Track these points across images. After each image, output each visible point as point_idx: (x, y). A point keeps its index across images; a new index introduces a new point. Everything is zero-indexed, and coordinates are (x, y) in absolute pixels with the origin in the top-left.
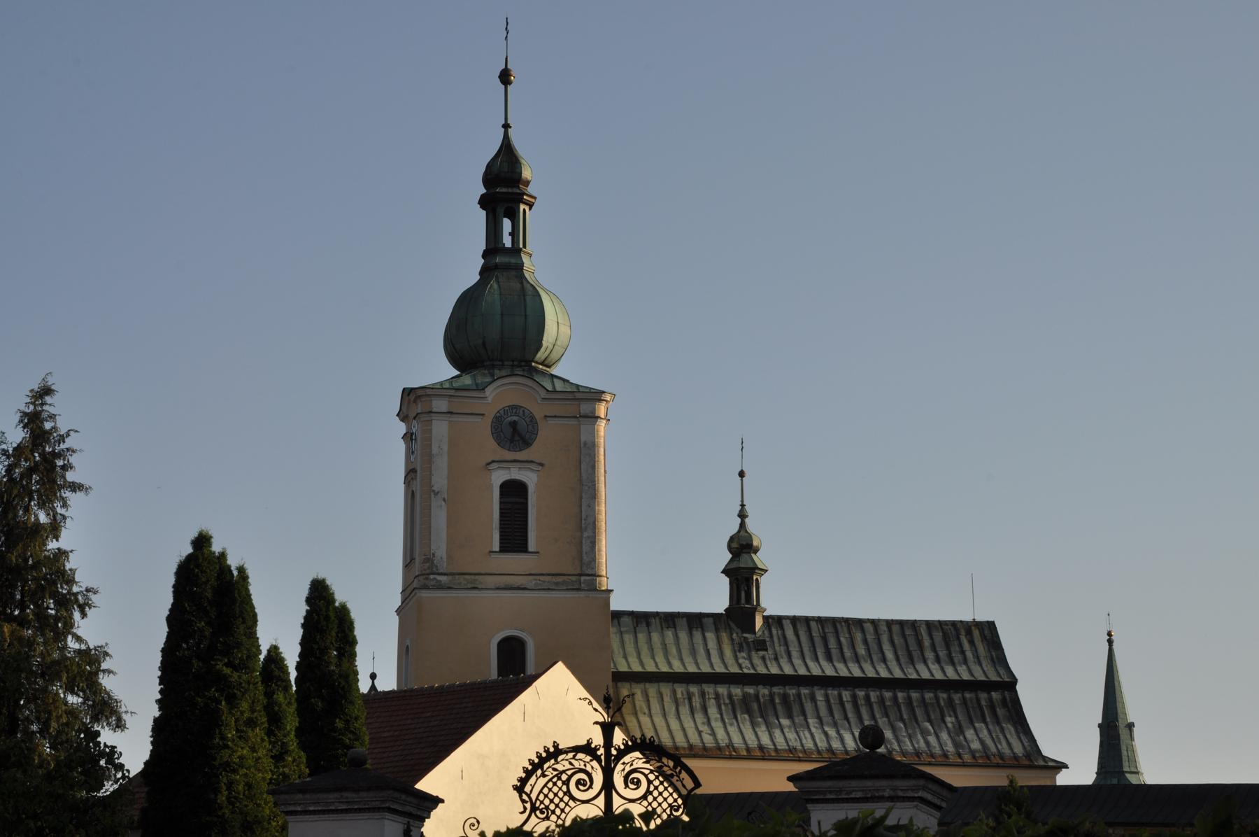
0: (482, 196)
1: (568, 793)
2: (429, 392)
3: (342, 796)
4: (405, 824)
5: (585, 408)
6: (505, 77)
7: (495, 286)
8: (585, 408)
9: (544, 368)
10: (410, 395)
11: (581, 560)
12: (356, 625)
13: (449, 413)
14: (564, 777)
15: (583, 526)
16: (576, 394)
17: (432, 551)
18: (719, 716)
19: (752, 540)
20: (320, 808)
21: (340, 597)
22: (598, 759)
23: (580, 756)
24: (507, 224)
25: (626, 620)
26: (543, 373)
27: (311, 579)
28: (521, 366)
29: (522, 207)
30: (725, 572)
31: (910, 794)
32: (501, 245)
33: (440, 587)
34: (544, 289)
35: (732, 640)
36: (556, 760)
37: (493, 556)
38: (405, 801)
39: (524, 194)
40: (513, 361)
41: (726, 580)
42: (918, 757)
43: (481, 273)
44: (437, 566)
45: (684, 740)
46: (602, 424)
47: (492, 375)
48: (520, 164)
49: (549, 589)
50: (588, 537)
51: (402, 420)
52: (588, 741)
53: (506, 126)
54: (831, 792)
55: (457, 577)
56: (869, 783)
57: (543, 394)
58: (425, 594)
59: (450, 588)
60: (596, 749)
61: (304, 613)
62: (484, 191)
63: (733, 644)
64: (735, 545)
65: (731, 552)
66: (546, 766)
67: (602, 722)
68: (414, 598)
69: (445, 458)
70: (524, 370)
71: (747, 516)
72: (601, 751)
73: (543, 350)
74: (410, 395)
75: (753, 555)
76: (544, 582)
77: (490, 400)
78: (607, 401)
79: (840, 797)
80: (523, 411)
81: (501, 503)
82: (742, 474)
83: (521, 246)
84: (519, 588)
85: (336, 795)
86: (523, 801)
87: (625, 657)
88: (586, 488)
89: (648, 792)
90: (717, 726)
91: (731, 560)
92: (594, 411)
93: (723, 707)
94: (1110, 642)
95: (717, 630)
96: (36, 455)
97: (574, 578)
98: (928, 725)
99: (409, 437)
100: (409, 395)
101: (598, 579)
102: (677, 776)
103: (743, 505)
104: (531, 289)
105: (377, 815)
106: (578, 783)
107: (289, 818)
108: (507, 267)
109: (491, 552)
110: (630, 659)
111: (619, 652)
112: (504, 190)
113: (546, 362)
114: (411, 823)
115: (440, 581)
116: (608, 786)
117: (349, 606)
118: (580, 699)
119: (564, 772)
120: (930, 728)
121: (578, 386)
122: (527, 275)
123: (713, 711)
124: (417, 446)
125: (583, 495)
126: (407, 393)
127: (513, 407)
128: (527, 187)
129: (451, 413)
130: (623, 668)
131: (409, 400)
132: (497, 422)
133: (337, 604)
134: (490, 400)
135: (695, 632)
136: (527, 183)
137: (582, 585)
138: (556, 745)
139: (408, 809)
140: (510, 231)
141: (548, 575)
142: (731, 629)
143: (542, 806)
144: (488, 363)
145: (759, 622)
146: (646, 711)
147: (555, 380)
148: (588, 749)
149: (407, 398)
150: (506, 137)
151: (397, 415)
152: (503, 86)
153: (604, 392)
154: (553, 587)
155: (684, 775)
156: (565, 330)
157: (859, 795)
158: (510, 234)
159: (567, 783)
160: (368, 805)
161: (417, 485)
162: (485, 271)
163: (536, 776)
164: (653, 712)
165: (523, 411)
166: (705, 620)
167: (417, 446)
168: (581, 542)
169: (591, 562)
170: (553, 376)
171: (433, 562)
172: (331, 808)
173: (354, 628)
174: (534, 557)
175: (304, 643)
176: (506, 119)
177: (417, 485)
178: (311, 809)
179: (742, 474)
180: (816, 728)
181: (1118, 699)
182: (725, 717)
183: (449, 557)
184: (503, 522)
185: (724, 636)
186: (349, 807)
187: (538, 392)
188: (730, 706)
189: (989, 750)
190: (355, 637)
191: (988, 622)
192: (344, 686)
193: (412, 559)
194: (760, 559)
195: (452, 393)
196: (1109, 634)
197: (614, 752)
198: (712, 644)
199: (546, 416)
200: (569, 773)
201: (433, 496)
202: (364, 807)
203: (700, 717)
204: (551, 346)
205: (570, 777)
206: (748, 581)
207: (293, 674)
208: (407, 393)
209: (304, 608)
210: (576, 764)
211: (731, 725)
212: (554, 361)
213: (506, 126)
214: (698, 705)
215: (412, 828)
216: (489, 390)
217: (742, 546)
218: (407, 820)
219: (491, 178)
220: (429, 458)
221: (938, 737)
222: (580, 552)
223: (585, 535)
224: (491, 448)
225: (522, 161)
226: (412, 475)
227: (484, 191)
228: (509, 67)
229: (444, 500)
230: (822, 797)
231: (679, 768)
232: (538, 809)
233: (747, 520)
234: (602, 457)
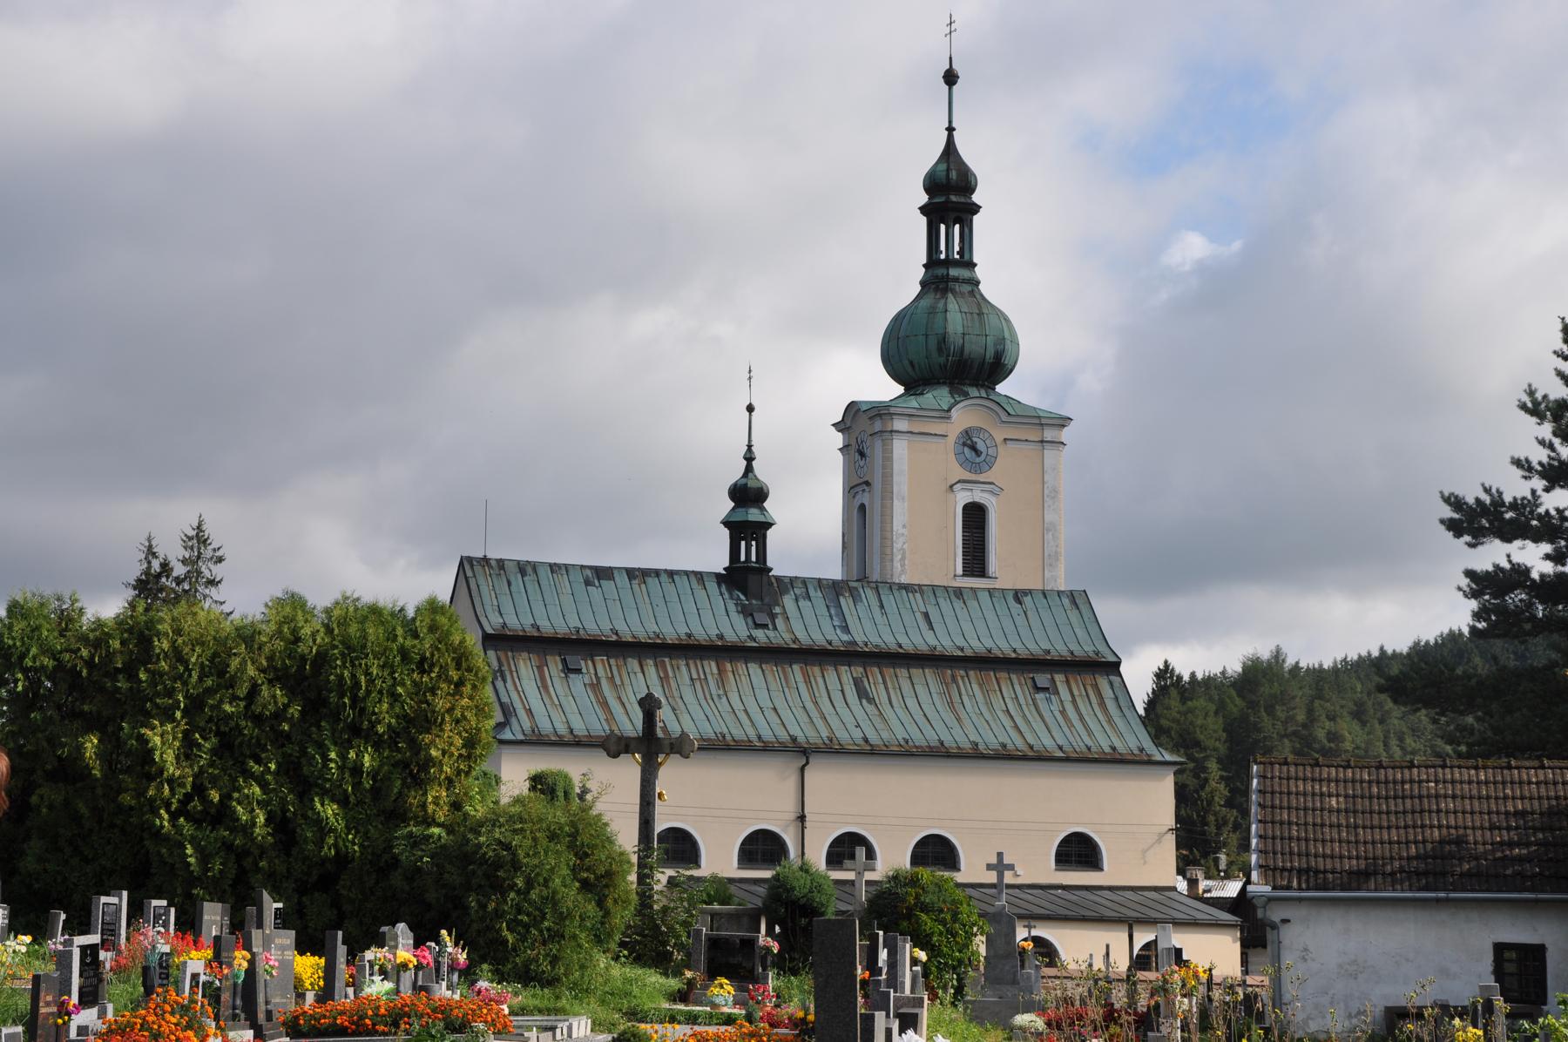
5: (1049, 434)
13: (908, 432)
30: (726, 523)
53: (950, 129)
71: (754, 459)
82: (750, 409)
96: (292, 809)
103: (750, 446)
150: (950, 144)
179: (750, 409)
199: (1005, 439)
213: (950, 129)
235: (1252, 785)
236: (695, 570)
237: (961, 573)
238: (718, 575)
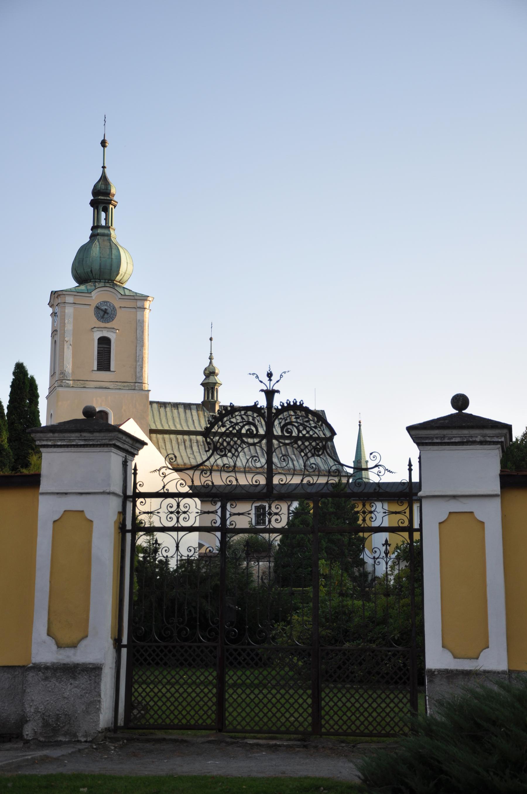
0: (92, 200)
2: (64, 293)
3: (81, 435)
4: (123, 457)
5: (139, 304)
6: (103, 143)
7: (97, 244)
8: (139, 304)
9: (120, 284)
10: (55, 295)
11: (136, 376)
12: (39, 387)
13: (74, 303)
15: (137, 360)
16: (135, 297)
18: (198, 450)
19: (215, 370)
20: (65, 443)
21: (31, 372)
23: (250, 413)
24: (103, 215)
25: (155, 406)
26: (119, 286)
27: (15, 363)
28: (108, 283)
29: (111, 206)
30: (202, 384)
31: (496, 439)
32: (100, 224)
33: (68, 386)
34: (120, 246)
35: (205, 416)
36: (232, 416)
37: (94, 372)
38: (125, 441)
39: (112, 200)
40: (105, 280)
41: (202, 388)
42: (289, 471)
43: (90, 237)
45: (181, 461)
46: (147, 312)
47: (95, 286)
48: (110, 185)
50: (140, 365)
51: (51, 307)
52: (255, 403)
53: (104, 167)
54: (437, 438)
56: (466, 432)
57: (120, 296)
58: (60, 389)
61: (12, 380)
62: (92, 198)
63: (205, 418)
64: (207, 372)
65: (205, 375)
66: (225, 419)
67: (266, 390)
68: (55, 391)
70: (110, 285)
71: (213, 359)
73: (120, 275)
74: (55, 295)
75: (215, 377)
76: (118, 385)
78: (150, 301)
79: (444, 441)
81: (98, 347)
82: (211, 339)
83: (110, 225)
85: (77, 435)
87: (155, 422)
88: (139, 342)
90: (197, 455)
91: (205, 379)
92: (144, 305)
93: (200, 446)
94: (360, 425)
95: (197, 411)
97: (132, 384)
98: (293, 456)
99: (54, 314)
100: (54, 294)
101: (144, 385)
102: (319, 427)
103: (211, 354)
104: (115, 246)
105: (106, 449)
108: (103, 235)
110: (157, 423)
111: (152, 420)
112: (102, 198)
113: (121, 282)
114: (127, 458)
115: (68, 383)
117: (35, 377)
118: (250, 374)
119: (237, 424)
120: (294, 458)
121: (136, 293)
122: (113, 239)
123: (195, 448)
124: (57, 319)
126: (53, 293)
127: (105, 302)
128: (113, 197)
129: (75, 303)
130: (153, 427)
131: (54, 296)
132: (97, 308)
133: (29, 376)
134: (94, 298)
135: (187, 411)
136: (114, 195)
139: (126, 447)
141: (120, 382)
142: (204, 411)
143: (222, 447)
144: (93, 280)
145: (217, 408)
146: (164, 447)
147: (125, 290)
148: (254, 408)
149: (53, 296)
150: (104, 172)
151: (48, 304)
152: (103, 148)
153: (148, 296)
156: (130, 267)
157: (458, 440)
160: (100, 442)
161: (57, 338)
162: (93, 237)
163: (218, 426)
164: (167, 448)
166: (192, 407)
167: (57, 319)
168: (136, 367)
169: (140, 377)
170: (124, 288)
171: (65, 374)
172: (73, 443)
173: (37, 389)
175: (12, 395)
176: (104, 164)
177: (57, 338)
178: (59, 443)
179: (211, 339)
180: (243, 457)
181: (362, 450)
182: (201, 451)
183: (73, 372)
185: (201, 413)
186: (86, 443)
188: (203, 446)
189: (321, 468)
190: (38, 393)
191: (321, 410)
192: (32, 418)
193: (54, 373)
194: (219, 379)
195: (76, 294)
196: (360, 422)
197: (274, 411)
198: (195, 418)
199: (120, 307)
200: (241, 424)
202: (97, 443)
203: (189, 450)
204: (123, 274)
206: (213, 389)
207: (6, 411)
208: (53, 293)
209: (11, 377)
211: (204, 455)
212: (125, 281)
213: (104, 167)
214: (188, 445)
215: (128, 460)
216: (93, 293)
217: (210, 373)
218: (124, 454)
219: (96, 192)
220: (63, 324)
221: (298, 462)
222: (136, 372)
223: (138, 364)
224: (94, 322)
225: (111, 184)
226: (55, 332)
227: (92, 198)
228: (105, 139)
230: (430, 441)
231: (320, 422)
232: (219, 448)
233: (213, 361)
234: (147, 327)
235: (282, 439)
236: (160, 401)
237: (96, 369)
238: (197, 405)
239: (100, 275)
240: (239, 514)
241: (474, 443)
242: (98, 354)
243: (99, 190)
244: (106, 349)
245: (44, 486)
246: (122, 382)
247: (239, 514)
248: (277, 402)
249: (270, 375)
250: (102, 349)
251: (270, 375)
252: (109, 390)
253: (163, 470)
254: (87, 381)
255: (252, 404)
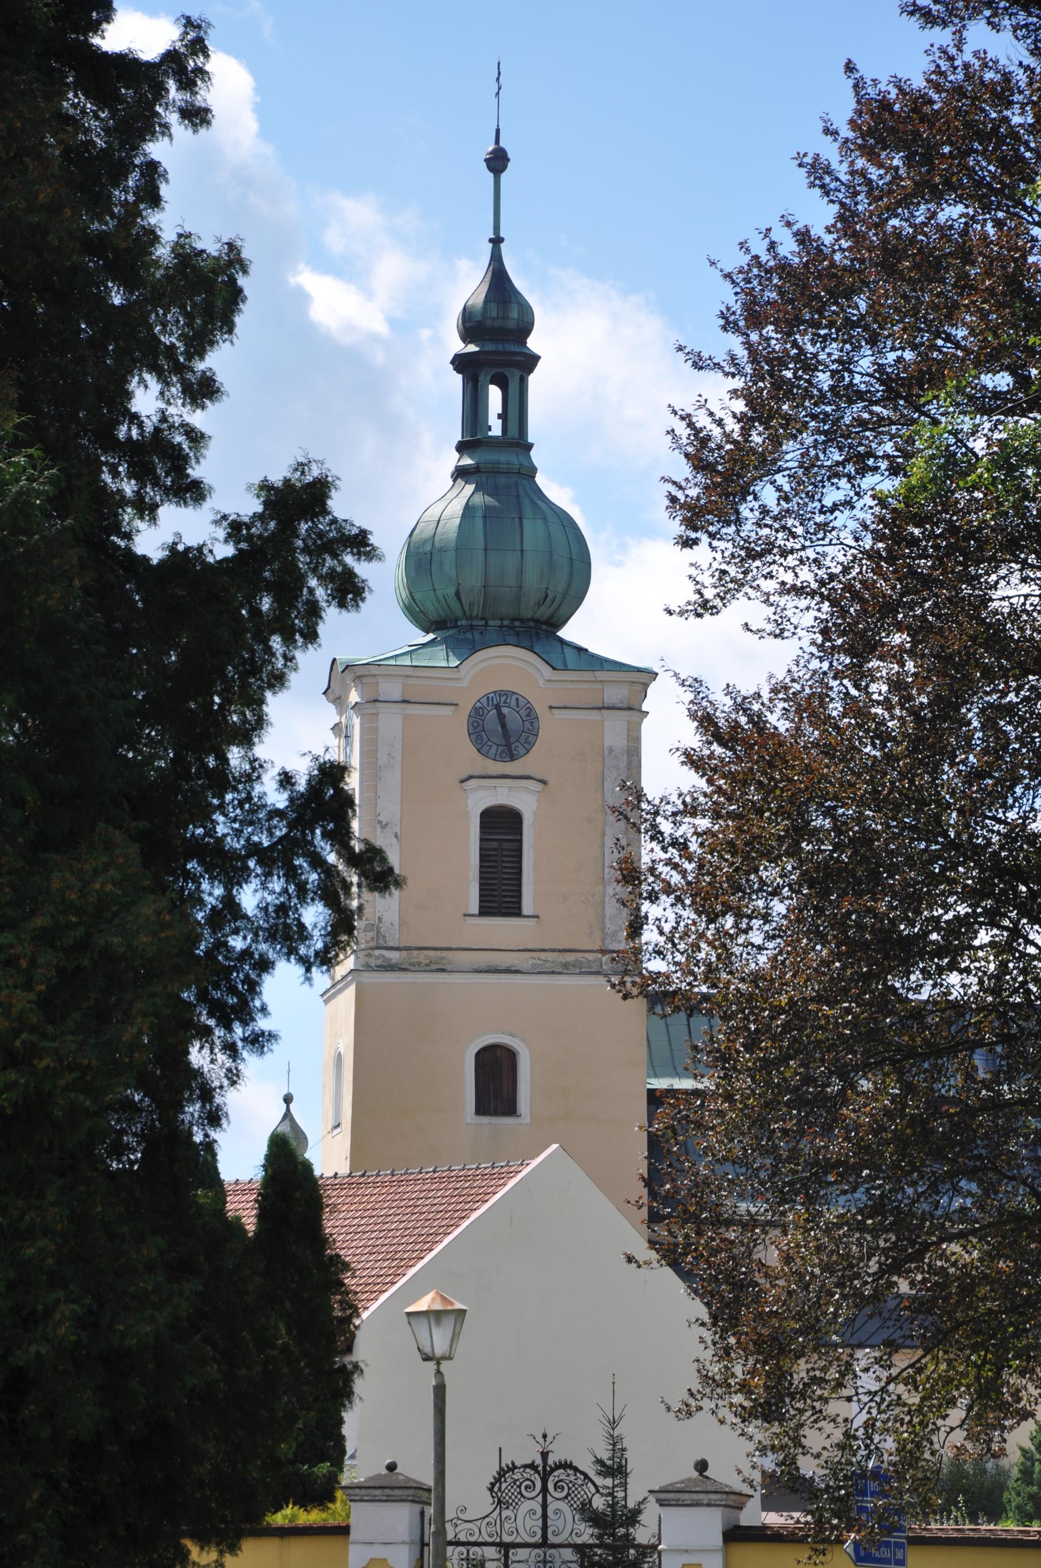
1: (520, 1493)
2: (374, 670)
11: (603, 929)
14: (518, 1483)
17: (378, 914)
22: (538, 1472)
23: (528, 1470)
24: (495, 394)
40: (502, 619)
44: (384, 937)
49: (553, 973)
53: (497, 241)
55: (415, 952)
59: (405, 970)
60: (538, 1466)
69: (398, 772)
72: (540, 1468)
76: (546, 961)
77: (465, 683)
80: (517, 699)
84: (508, 971)
86: (493, 1497)
89: (568, 1494)
106: (526, 1487)
107: (352, 1504)
109: (465, 915)
113: (553, 621)
116: (544, 1490)
125: (607, 829)
129: (408, 702)
137: (604, 967)
138: (513, 1463)
140: (500, 412)
147: (566, 649)
148: (532, 1466)
154: (560, 970)
155: (590, 1485)
157: (689, 1502)
158: (500, 416)
159: (519, 1487)
165: (517, 699)
168: (603, 902)
174: (532, 922)
176: (497, 141)
183: (402, 922)
184: (484, 893)
187: (541, 673)
199: (551, 707)
201: (379, 830)
205: (521, 1483)
210: (525, 1475)
213: (497, 241)
224: (469, 757)
229: (396, 836)
239: (484, 605)
240: (519, 1562)
241: (702, 1505)
242: (481, 861)
243: (479, 322)
244: (506, 845)
245: (354, 1535)
246: (560, 951)
247: (519, 1562)
248: (550, 1462)
249: (545, 1436)
250: (494, 844)
251: (545, 1436)
252: (518, 976)
253: (455, 1521)
254: (450, 949)
255: (530, 1462)
